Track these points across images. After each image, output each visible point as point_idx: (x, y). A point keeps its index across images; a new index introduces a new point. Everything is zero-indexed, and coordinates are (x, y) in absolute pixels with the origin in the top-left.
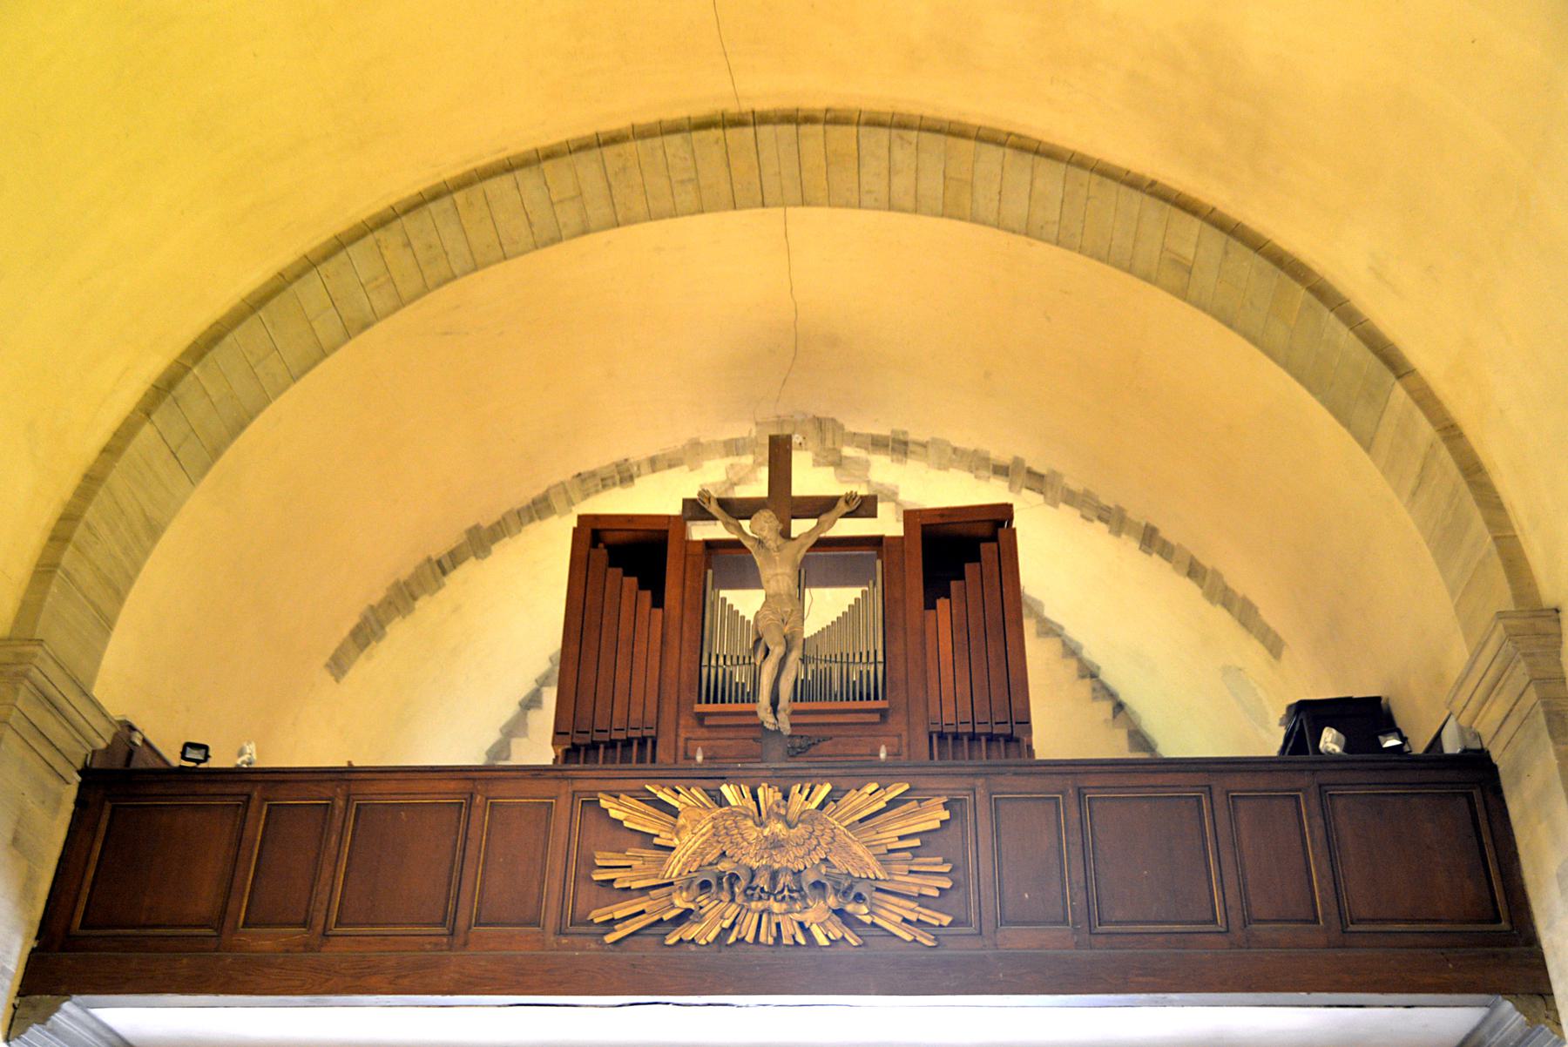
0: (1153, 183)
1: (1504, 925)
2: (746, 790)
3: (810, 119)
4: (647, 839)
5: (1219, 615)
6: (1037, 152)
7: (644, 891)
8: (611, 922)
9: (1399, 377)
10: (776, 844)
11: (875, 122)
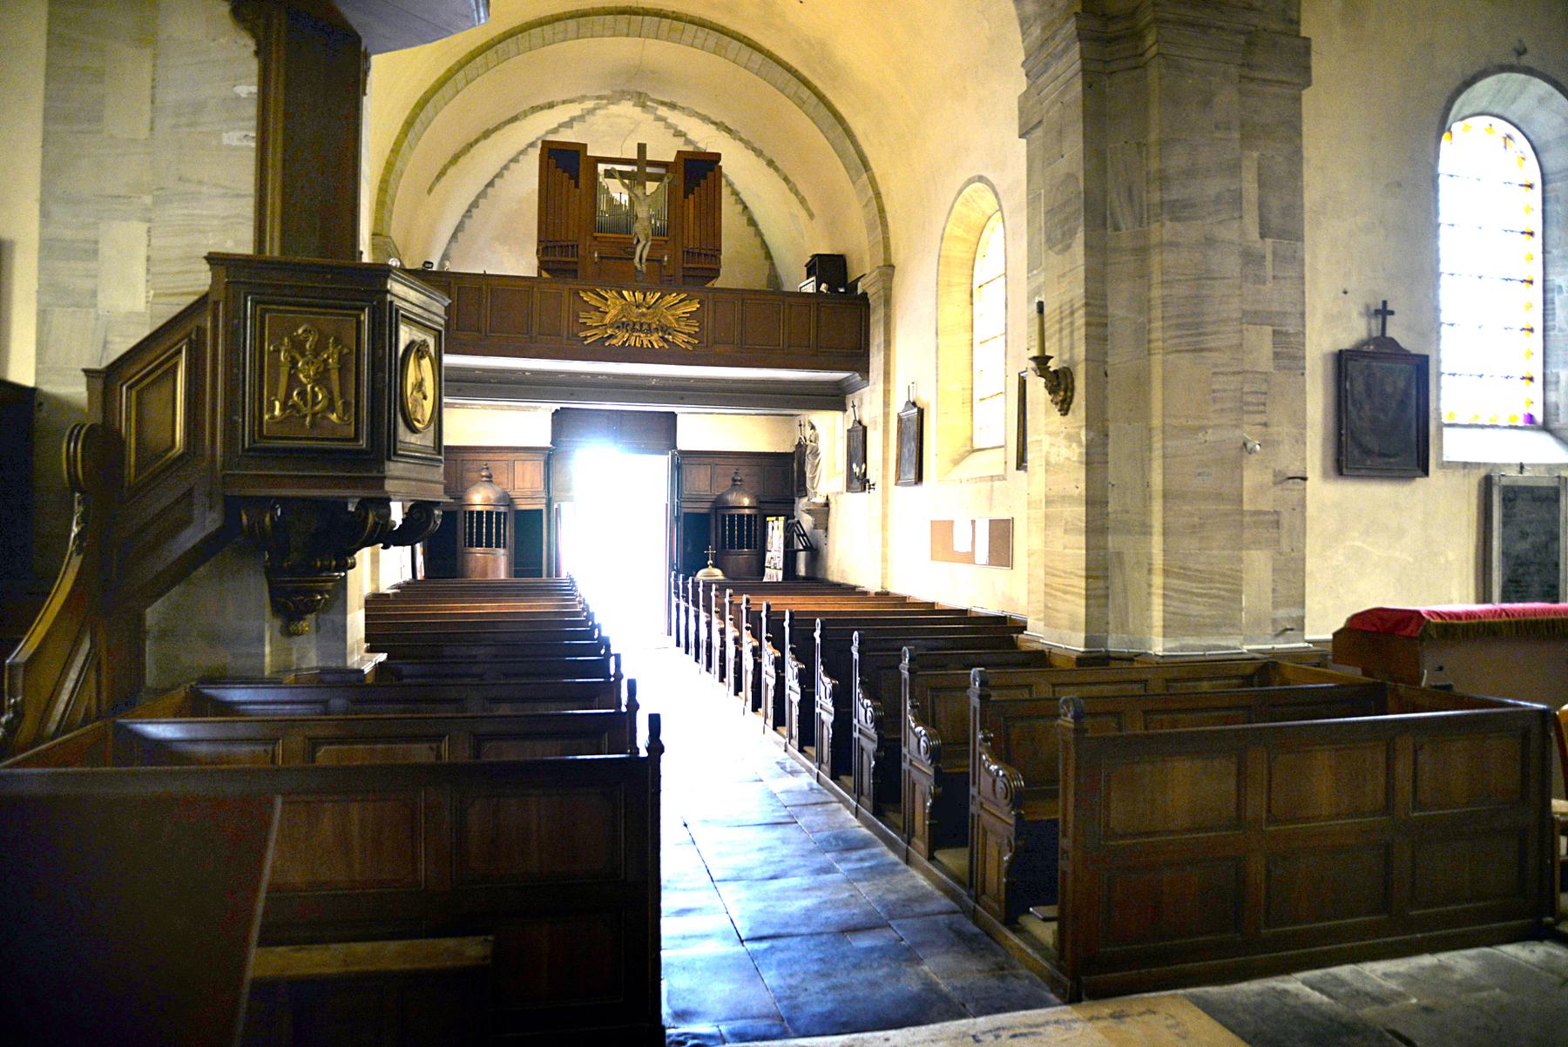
3: (665, 16)
4: (597, 309)
5: (793, 196)
8: (586, 338)
10: (643, 315)
11: (692, 22)
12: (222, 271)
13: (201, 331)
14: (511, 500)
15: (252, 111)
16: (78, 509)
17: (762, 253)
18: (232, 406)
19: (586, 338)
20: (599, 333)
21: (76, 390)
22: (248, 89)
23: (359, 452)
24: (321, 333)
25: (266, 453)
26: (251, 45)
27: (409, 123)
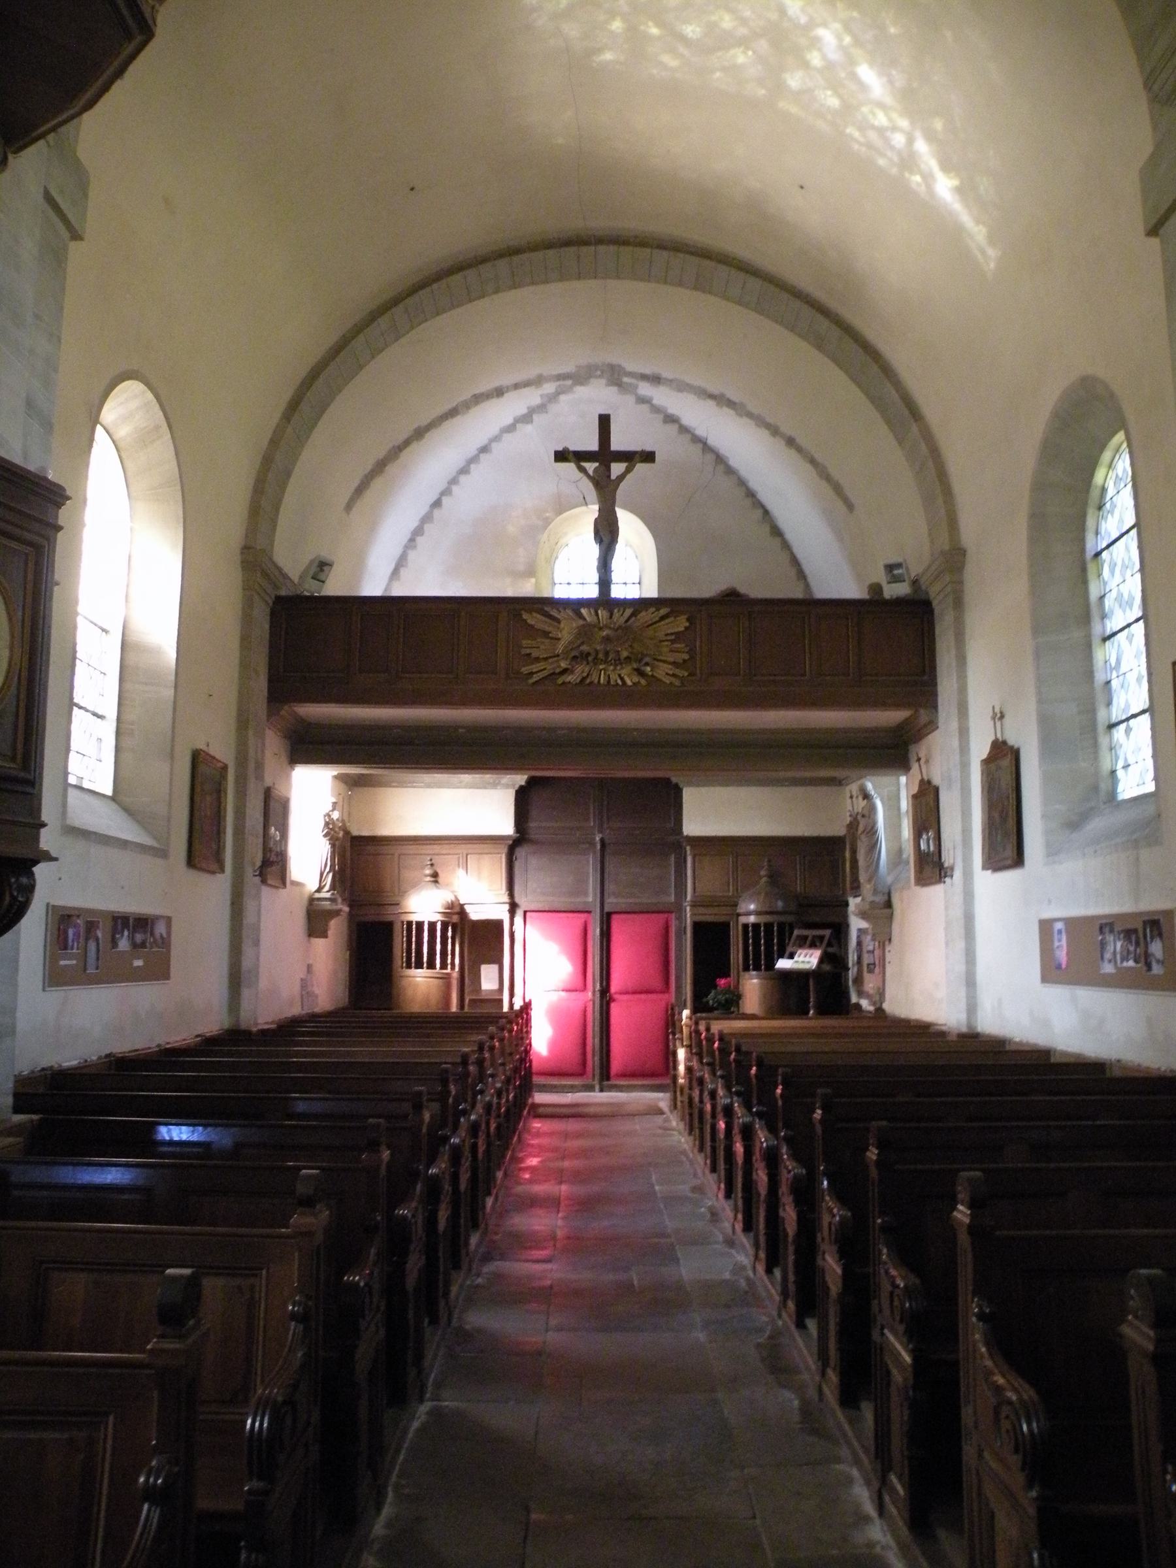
0: (807, 295)
1: (925, 678)
2: (592, 611)
4: (546, 634)
6: (747, 272)
7: (546, 659)
8: (531, 674)
9: (916, 421)
14: (462, 906)
17: (793, 573)
19: (531, 674)
20: (549, 667)
27: (294, 406)
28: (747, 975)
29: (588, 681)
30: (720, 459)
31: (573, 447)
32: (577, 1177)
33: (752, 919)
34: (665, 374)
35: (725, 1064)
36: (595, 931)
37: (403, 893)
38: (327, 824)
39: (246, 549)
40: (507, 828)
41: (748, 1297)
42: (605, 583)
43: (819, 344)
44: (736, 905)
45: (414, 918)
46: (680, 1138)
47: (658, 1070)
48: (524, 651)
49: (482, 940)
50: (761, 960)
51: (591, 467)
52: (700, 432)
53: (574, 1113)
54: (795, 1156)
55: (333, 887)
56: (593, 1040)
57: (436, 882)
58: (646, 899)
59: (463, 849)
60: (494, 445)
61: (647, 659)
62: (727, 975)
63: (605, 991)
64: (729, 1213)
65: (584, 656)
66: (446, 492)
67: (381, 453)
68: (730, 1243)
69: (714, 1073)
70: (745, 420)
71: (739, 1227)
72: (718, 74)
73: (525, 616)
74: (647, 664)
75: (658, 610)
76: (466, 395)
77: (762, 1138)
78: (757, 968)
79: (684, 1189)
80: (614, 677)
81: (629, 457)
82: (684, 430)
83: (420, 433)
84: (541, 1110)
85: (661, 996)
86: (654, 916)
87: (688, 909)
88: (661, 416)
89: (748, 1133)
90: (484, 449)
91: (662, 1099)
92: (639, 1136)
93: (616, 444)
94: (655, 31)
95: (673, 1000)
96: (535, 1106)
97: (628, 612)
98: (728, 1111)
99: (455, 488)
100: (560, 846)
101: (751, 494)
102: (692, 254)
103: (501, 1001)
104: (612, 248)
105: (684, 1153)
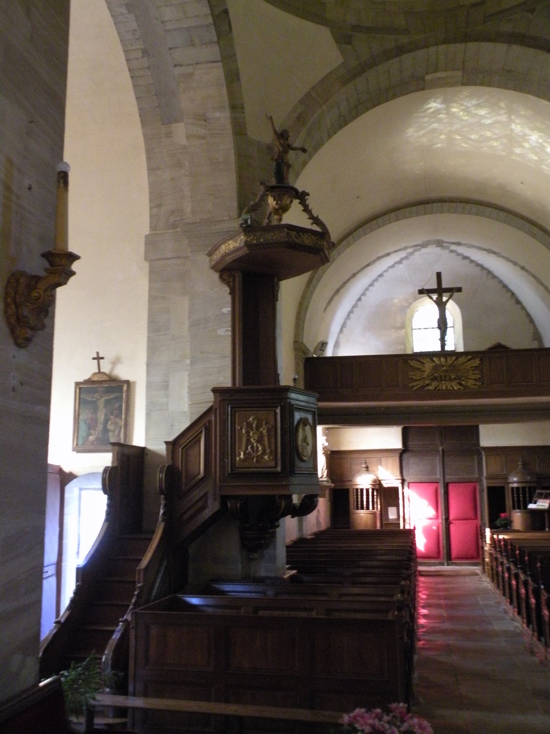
4: (419, 369)
7: (420, 380)
8: (413, 387)
12: (218, 394)
13: (210, 422)
14: (380, 481)
15: (229, 318)
16: (163, 502)
18: (223, 455)
20: (421, 383)
21: (160, 448)
22: (227, 310)
23: (279, 473)
24: (258, 419)
25: (238, 475)
26: (228, 290)
28: (514, 511)
29: (438, 389)
30: (489, 272)
31: (426, 288)
32: (446, 598)
33: (515, 485)
34: (463, 242)
35: (506, 550)
36: (441, 491)
37: (353, 476)
38: (324, 448)
39: (295, 342)
40: (398, 445)
41: (521, 634)
42: (443, 345)
43: (534, 236)
44: (507, 479)
45: (359, 487)
46: (487, 583)
47: (474, 554)
48: (410, 377)
49: (389, 496)
50: (521, 504)
51: (435, 297)
52: (480, 262)
53: (438, 574)
54: (533, 581)
55: (327, 476)
56: (443, 541)
57: (367, 470)
58: (466, 476)
59: (379, 455)
60: (385, 274)
61: (463, 379)
62: (504, 511)
63: (447, 519)
64: (512, 610)
65: (435, 379)
66: (364, 294)
67: (339, 285)
68: (513, 620)
69: (502, 555)
70: (501, 259)
71: (516, 614)
72: (485, 149)
73: (410, 362)
74: (463, 381)
75: (467, 357)
76: (374, 257)
77: (522, 577)
78: (519, 508)
79: (492, 603)
80: (449, 386)
81: (450, 290)
82: (472, 261)
83: (354, 275)
84: (423, 573)
85: (474, 521)
86: (467, 484)
87: (484, 480)
88: (461, 257)
89: (517, 576)
90: (381, 276)
91: (477, 569)
92: (470, 584)
93: (444, 285)
94: (458, 137)
95: (480, 523)
96: (420, 572)
97: (454, 358)
98: (509, 569)
99: (367, 292)
100: (423, 453)
101: (505, 286)
102: (475, 204)
103: (399, 524)
104: (440, 204)
105: (490, 590)
